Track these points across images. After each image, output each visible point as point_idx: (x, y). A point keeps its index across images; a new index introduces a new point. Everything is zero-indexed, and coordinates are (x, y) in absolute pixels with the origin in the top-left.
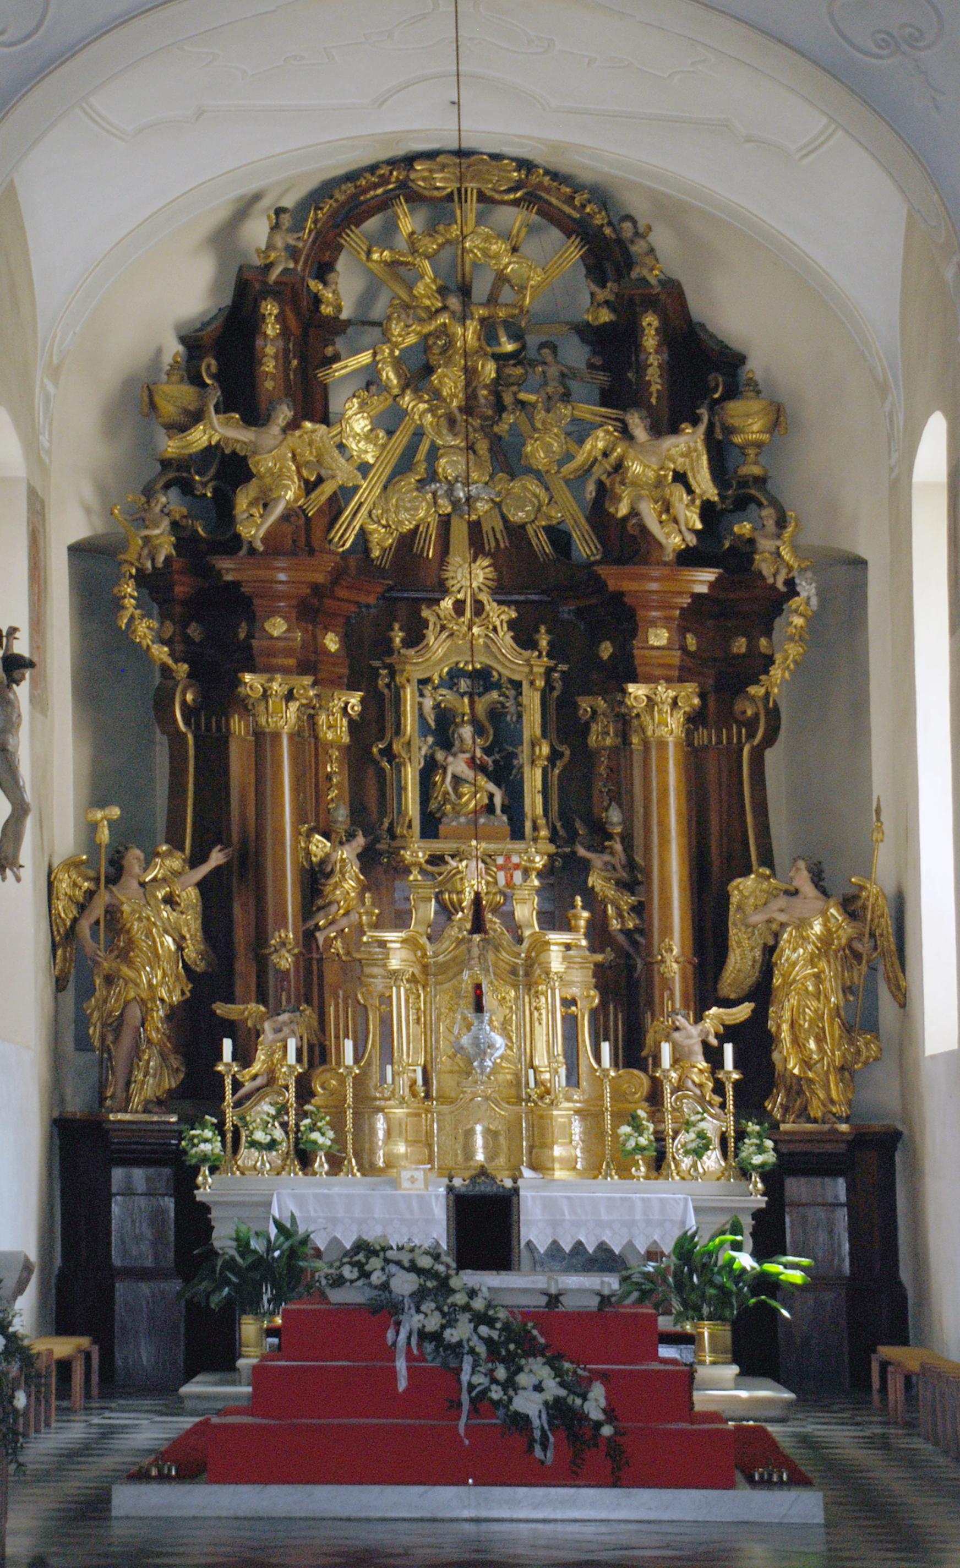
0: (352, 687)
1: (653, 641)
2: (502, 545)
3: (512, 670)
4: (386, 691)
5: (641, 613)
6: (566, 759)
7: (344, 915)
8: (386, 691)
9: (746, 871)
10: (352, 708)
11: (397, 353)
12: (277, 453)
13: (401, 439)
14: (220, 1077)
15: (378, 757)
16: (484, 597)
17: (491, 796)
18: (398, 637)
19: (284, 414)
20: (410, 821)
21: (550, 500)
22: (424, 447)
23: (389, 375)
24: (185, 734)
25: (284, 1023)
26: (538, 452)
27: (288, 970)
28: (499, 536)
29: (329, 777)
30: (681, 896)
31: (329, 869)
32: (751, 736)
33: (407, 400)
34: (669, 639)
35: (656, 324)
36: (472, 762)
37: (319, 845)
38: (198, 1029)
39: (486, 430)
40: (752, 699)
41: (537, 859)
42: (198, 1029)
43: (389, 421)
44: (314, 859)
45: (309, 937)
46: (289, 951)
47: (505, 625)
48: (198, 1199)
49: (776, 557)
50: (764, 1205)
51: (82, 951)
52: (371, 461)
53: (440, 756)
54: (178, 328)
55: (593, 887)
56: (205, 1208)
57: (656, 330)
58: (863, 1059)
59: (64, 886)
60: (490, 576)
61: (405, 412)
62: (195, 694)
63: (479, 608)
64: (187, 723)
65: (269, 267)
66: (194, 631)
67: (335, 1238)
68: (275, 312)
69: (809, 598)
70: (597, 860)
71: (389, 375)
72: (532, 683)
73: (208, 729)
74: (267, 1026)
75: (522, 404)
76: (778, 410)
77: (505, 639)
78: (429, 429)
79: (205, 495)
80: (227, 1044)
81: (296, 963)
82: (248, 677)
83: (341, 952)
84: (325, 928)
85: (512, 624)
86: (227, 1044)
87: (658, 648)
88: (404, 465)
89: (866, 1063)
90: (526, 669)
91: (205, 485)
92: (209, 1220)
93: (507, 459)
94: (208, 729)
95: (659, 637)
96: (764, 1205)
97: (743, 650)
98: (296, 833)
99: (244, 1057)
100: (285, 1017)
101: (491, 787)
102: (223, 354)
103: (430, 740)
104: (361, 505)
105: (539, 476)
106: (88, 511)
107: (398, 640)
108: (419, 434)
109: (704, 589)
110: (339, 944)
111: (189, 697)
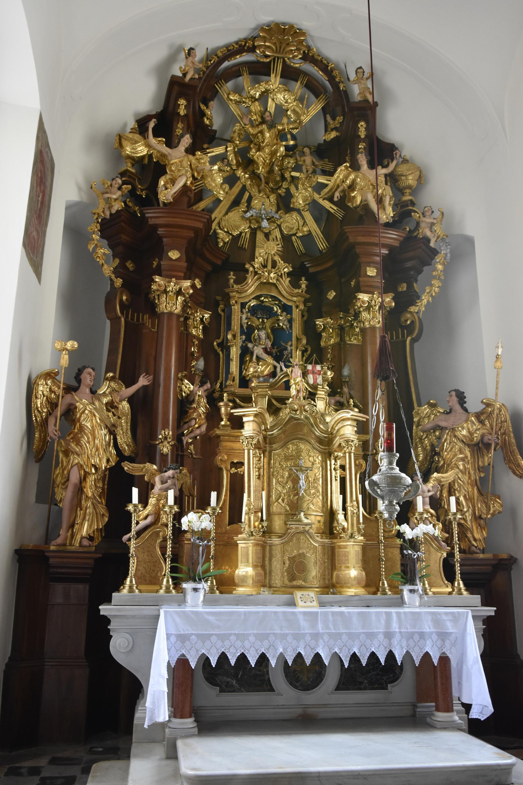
0: (206, 308)
1: (369, 273)
3: (288, 299)
4: (222, 314)
5: (363, 259)
7: (197, 428)
8: (222, 314)
10: (206, 319)
11: (236, 150)
12: (177, 156)
13: (236, 189)
14: (129, 514)
15: (216, 347)
16: (277, 258)
18: (232, 277)
19: (187, 140)
20: (234, 377)
21: (304, 224)
22: (246, 195)
23: (231, 157)
24: (120, 318)
25: (169, 478)
26: (299, 200)
27: (167, 454)
29: (192, 354)
31: (192, 399)
33: (240, 173)
34: (377, 272)
35: (365, 126)
36: (265, 350)
37: (188, 386)
38: (117, 485)
41: (329, 373)
42: (117, 485)
44: (183, 394)
45: (179, 438)
46: (169, 443)
47: (286, 275)
48: (102, 613)
50: (493, 614)
51: (45, 438)
52: (222, 199)
53: (250, 345)
54: (136, 115)
56: (106, 621)
57: (365, 128)
58: (491, 511)
59: (42, 388)
60: (280, 249)
61: (239, 179)
62: (126, 295)
63: (274, 264)
64: (122, 312)
65: (185, 75)
66: (130, 265)
68: (185, 104)
69: (446, 254)
71: (231, 157)
72: (297, 307)
73: (132, 319)
74: (157, 479)
75: (293, 177)
77: (286, 281)
78: (248, 186)
79: (142, 196)
80: (135, 491)
81: (172, 450)
82: (157, 279)
83: (193, 452)
84: (187, 435)
85: (289, 274)
86: (135, 491)
87: (372, 277)
88: (236, 203)
89: (493, 515)
90: (292, 295)
91: (142, 190)
92: (109, 630)
93: (285, 204)
94: (132, 319)
95: (371, 272)
96: (493, 614)
97: (405, 289)
98: (177, 379)
99: (144, 500)
100: (170, 473)
102: (161, 124)
103: (244, 337)
105: (298, 211)
106: (80, 189)
107: (232, 281)
108: (244, 189)
110: (192, 447)
111: (124, 298)
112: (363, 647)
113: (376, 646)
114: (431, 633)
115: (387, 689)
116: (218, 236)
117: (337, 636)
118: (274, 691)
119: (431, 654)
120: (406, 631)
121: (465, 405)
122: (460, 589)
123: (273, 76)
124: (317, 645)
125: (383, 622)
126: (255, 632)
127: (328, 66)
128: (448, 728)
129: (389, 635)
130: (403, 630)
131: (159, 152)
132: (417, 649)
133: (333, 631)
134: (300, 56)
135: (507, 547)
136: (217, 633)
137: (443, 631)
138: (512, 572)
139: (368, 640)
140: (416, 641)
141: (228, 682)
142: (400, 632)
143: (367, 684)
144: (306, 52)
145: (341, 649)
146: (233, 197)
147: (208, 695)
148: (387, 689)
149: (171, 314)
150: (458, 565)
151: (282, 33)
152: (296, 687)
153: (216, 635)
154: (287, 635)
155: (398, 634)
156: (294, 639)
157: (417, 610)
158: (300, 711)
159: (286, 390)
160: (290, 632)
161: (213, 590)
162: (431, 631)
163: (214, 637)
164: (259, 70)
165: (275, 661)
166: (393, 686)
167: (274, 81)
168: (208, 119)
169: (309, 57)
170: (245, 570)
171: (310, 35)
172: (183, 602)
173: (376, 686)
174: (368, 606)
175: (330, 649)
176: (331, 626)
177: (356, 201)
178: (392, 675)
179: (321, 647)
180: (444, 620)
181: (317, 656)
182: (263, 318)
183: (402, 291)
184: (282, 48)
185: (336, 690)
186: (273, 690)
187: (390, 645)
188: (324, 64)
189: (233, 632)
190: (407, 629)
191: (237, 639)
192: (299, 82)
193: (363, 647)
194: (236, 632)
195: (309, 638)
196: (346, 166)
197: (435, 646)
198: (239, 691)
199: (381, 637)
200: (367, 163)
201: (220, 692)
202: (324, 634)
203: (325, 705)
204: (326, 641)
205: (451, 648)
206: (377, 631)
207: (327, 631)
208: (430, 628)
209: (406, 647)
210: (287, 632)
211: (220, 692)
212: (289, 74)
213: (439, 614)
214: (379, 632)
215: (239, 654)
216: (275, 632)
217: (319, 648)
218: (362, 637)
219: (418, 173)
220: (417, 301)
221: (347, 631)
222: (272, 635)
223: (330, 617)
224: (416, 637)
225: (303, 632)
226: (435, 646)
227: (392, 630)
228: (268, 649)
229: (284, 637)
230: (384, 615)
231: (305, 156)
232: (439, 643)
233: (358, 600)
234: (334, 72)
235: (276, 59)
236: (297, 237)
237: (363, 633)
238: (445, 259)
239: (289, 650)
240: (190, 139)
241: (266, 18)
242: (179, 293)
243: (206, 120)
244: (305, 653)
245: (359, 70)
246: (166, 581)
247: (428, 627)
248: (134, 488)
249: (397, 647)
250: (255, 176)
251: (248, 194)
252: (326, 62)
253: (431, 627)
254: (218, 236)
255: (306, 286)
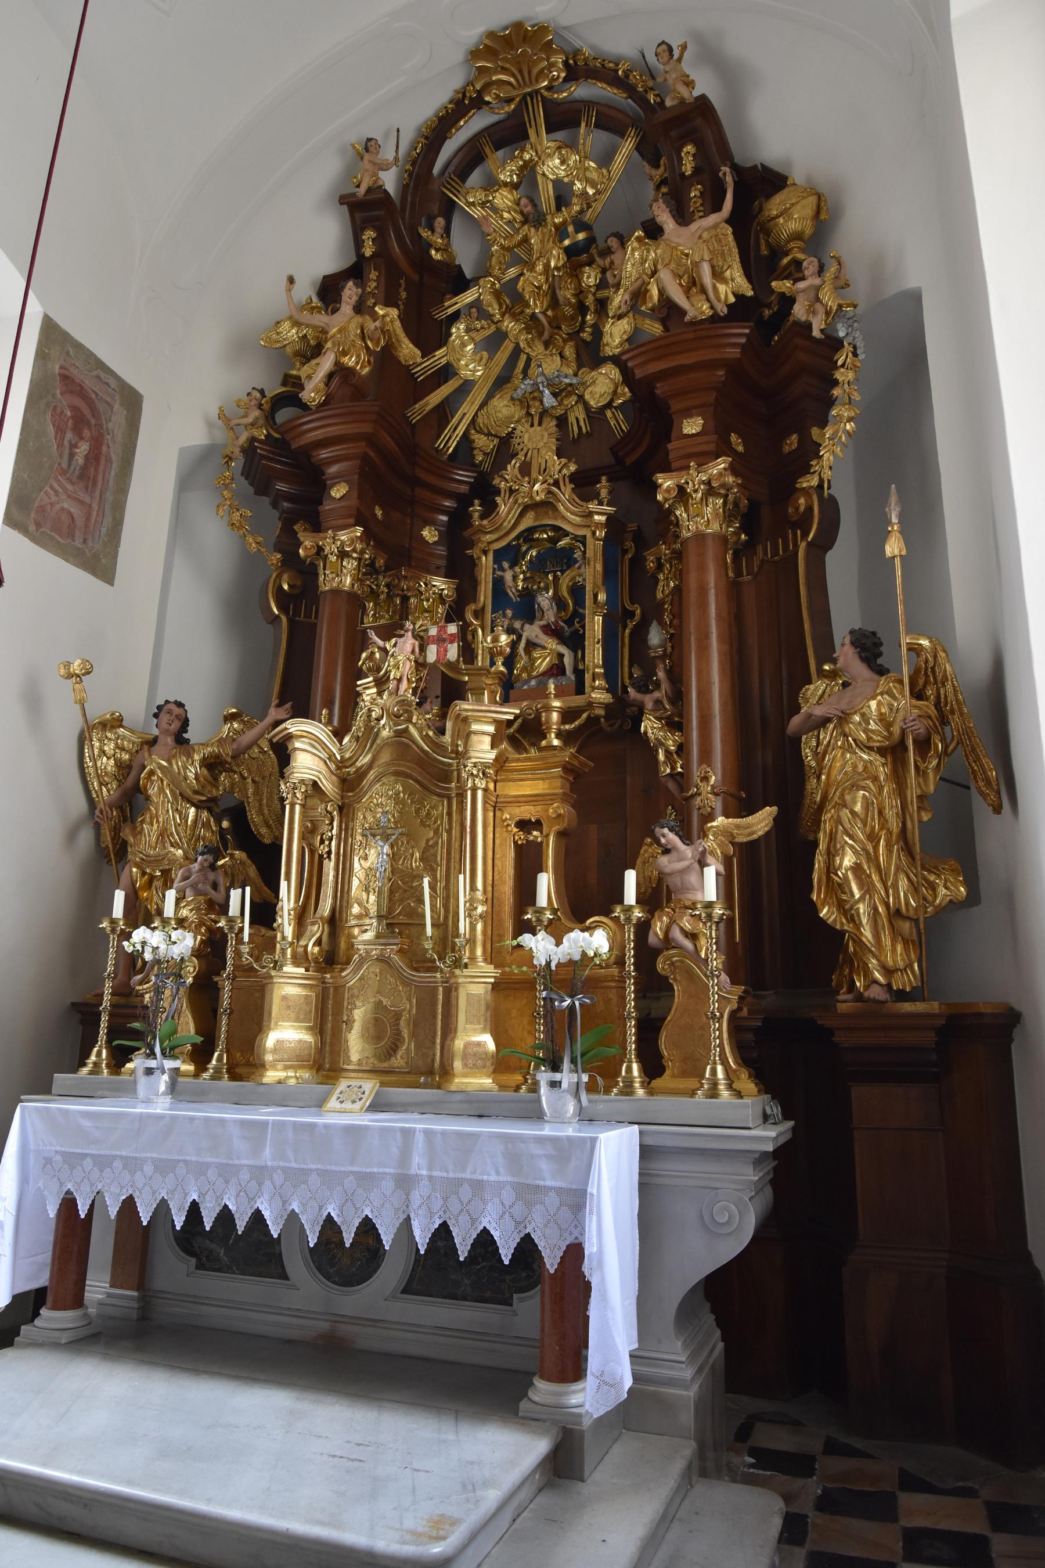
2: (584, 430)
5: (675, 405)
6: (637, 617)
9: (810, 682)
13: (502, 356)
17: (561, 656)
28: (582, 424)
30: (721, 682)
32: (805, 535)
33: (509, 325)
39: (574, 336)
40: (806, 492)
43: (494, 342)
47: (567, 480)
49: (811, 304)
55: (646, 732)
57: (694, 155)
67: (485, 1231)
70: (648, 701)
76: (819, 197)
77: (566, 494)
87: (693, 435)
88: (502, 381)
101: (562, 649)
104: (465, 414)
106: (210, 425)
107: (476, 515)
108: (517, 351)
109: (734, 353)
112: (349, 1203)
113: (375, 1204)
114: (500, 1186)
115: (511, 1305)
116: (474, 445)
117: (298, 1177)
118: (287, 1279)
119: (496, 1235)
120: (445, 1174)
121: (879, 661)
122: (714, 1084)
123: (531, 132)
124: (259, 1193)
125: (395, 1151)
126: (154, 1155)
127: (617, 71)
128: (544, 1421)
129: (405, 1182)
130: (435, 1174)
131: (315, 327)
132: (464, 1218)
133: (293, 1165)
134: (563, 75)
135: (981, 985)
136: (94, 1152)
137: (529, 1182)
138: (1013, 1046)
139: (360, 1191)
140: (465, 1200)
141: (212, 1251)
142: (431, 1178)
143: (469, 1289)
144: (571, 62)
145: (303, 1205)
146: (496, 371)
147: (172, 1270)
148: (511, 1305)
149: (336, 592)
150: (104, 1018)
151: (513, 45)
152: (328, 1277)
153: (92, 1156)
154: (208, 1165)
155: (426, 1182)
156: (220, 1175)
157: (570, 1131)
158: (324, 1326)
159: (577, 694)
160: (214, 1160)
161: (221, 1072)
162: (501, 1179)
163: (89, 1159)
164: (510, 134)
165: (184, 1218)
166: (521, 1300)
167: (542, 140)
168: (437, 250)
169: (578, 69)
170: (285, 1034)
171: (565, 28)
172: (130, 1090)
173: (488, 1294)
174: (480, 1116)
175: (284, 1202)
176: (291, 1154)
177: (651, 297)
178: (524, 1274)
179: (266, 1196)
180: (532, 1156)
181: (257, 1217)
182: (555, 572)
183: (790, 452)
184: (526, 74)
185: (404, 1292)
186: (286, 1278)
187: (407, 1206)
188: (610, 69)
189: (118, 1153)
190: (447, 1172)
191: (125, 1167)
192: (583, 125)
193: (349, 1203)
194: (124, 1154)
195: (247, 1177)
196: (639, 239)
197: (507, 1216)
198: (227, 1269)
199: (388, 1185)
200: (674, 217)
201: (197, 1268)
202: (274, 1169)
203: (375, 1322)
204: (278, 1183)
205: (546, 1226)
206: (381, 1170)
207: (282, 1164)
208: (498, 1173)
209: (441, 1213)
210: (209, 1160)
211: (197, 1268)
212: (563, 119)
213: (521, 1138)
214: (310, 1170)
215: (124, 1197)
216: (187, 1158)
217: (262, 1199)
218: (350, 1183)
219: (812, 200)
220: (814, 463)
221: (319, 1166)
222: (181, 1164)
223: (291, 1136)
224: (466, 1192)
225: (236, 1162)
226: (507, 1216)
227: (412, 1172)
228: (173, 1192)
229: (201, 1169)
230: (398, 1135)
231: (613, 253)
232: (518, 1210)
233: (461, 1102)
234: (631, 77)
235: (529, 98)
236: (615, 408)
237: (352, 1172)
238: (855, 354)
239: (208, 1197)
240: (354, 289)
241: (473, 34)
242: (343, 555)
243: (433, 252)
244: (238, 1208)
245: (660, 49)
246: (99, 1053)
247: (491, 1170)
248: (117, 892)
249: (420, 1212)
250: (533, 324)
251: (525, 356)
252: (611, 65)
253: (501, 1170)
254: (474, 445)
255: (610, 493)
